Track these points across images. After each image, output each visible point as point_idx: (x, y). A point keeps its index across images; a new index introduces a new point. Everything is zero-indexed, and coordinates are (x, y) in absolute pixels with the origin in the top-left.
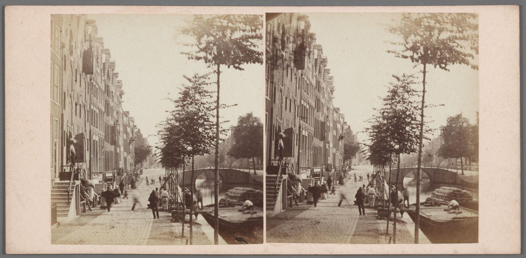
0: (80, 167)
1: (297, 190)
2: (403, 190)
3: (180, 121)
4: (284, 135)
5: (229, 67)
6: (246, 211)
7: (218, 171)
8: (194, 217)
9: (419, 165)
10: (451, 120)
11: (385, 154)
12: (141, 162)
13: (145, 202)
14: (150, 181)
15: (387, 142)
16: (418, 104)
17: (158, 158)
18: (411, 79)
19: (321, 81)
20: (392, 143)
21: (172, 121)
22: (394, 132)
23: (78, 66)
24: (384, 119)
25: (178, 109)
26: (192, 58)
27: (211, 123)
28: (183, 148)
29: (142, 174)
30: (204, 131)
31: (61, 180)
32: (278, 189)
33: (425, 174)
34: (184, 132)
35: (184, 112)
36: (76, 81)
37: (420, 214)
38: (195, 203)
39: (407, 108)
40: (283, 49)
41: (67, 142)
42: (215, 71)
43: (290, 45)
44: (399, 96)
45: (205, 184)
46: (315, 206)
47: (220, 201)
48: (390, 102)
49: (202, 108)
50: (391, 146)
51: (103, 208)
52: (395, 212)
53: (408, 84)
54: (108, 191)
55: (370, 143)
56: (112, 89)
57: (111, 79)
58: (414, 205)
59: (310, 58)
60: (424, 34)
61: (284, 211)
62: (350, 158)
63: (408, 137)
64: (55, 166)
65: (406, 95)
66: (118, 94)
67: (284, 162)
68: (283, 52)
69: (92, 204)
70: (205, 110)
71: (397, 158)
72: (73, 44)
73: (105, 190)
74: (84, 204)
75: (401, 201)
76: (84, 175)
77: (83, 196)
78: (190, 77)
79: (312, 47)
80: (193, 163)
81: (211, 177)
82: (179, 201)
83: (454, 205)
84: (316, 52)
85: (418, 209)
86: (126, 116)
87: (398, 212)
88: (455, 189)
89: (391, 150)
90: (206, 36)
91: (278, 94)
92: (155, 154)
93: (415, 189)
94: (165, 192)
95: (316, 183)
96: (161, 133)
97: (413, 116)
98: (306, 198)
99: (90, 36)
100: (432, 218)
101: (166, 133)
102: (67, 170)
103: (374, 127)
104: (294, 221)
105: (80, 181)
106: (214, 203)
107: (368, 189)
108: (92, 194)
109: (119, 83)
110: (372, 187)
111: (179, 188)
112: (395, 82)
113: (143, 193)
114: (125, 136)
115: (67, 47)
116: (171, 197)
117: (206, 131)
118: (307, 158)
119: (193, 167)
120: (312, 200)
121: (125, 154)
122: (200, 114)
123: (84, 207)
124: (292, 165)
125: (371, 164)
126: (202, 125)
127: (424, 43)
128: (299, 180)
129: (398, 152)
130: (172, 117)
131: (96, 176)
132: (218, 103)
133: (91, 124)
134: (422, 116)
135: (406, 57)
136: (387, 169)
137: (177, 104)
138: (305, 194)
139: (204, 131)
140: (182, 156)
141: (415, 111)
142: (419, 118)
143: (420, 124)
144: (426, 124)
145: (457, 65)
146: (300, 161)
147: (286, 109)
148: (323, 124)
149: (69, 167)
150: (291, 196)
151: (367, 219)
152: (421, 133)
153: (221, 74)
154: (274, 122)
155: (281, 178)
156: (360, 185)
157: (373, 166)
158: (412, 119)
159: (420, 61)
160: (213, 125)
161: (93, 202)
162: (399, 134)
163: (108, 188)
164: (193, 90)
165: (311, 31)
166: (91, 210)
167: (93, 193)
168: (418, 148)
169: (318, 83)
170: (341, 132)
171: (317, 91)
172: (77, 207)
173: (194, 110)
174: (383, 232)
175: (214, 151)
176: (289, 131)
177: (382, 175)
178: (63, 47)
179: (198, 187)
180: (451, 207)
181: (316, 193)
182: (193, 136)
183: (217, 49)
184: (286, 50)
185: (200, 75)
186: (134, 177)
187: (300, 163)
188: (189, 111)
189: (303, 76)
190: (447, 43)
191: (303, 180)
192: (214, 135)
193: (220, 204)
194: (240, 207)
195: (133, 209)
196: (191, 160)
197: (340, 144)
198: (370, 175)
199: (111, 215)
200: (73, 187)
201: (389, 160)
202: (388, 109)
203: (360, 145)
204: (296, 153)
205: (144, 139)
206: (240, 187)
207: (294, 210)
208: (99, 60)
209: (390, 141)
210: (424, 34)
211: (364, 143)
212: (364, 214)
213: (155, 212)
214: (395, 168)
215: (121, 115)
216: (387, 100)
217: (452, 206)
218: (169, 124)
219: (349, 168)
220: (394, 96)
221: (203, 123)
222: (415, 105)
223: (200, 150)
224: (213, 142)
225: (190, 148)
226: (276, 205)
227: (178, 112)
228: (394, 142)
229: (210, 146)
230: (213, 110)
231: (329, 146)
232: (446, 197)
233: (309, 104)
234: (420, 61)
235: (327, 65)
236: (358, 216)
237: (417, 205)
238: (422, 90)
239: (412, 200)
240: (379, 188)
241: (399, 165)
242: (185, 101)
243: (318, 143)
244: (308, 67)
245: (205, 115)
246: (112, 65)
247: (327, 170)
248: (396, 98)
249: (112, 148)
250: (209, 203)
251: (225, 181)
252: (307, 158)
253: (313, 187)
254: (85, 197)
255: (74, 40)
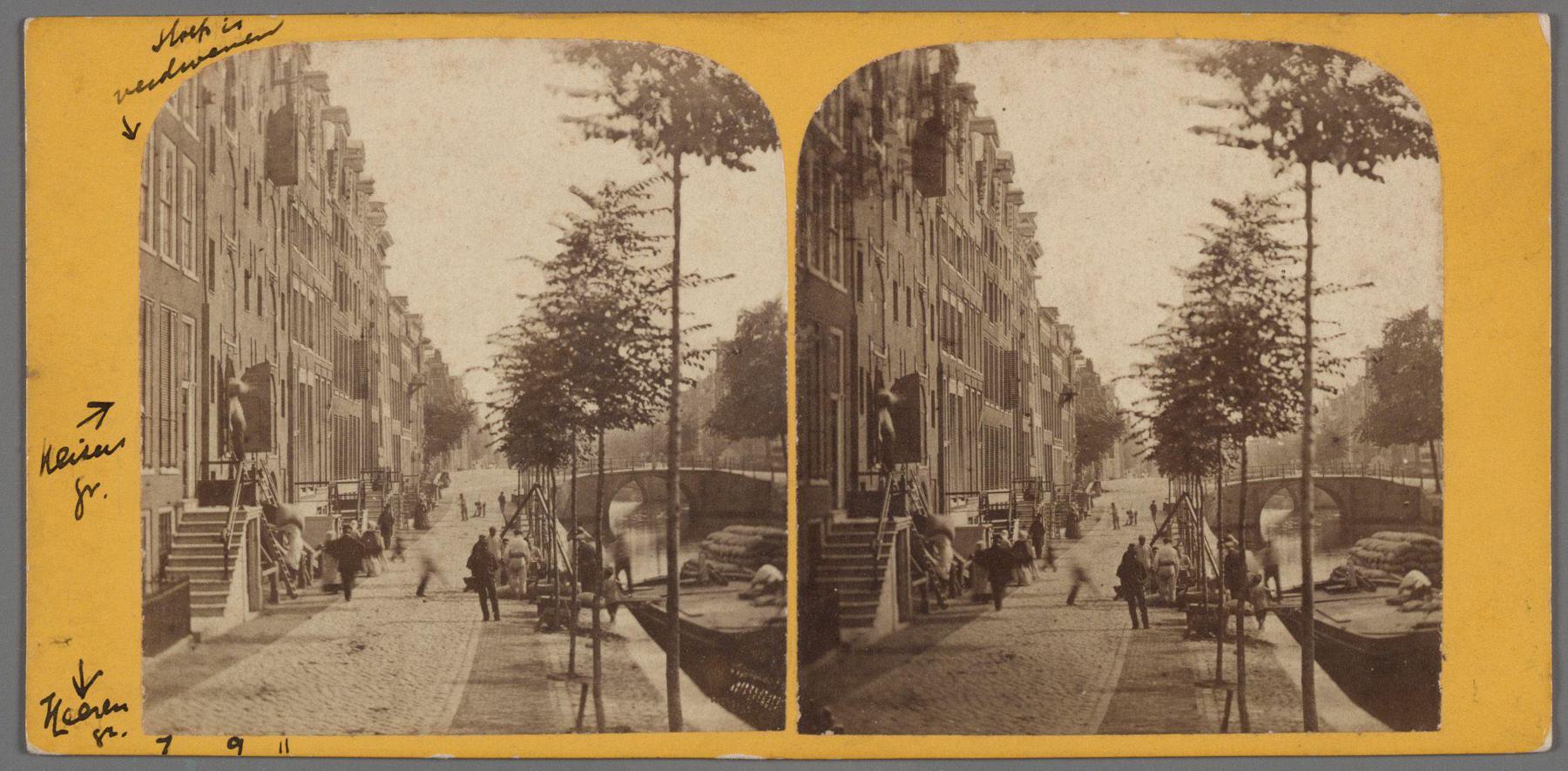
0: (259, 467)
1: (941, 562)
2: (1260, 545)
3: (561, 327)
4: (893, 398)
5: (708, 162)
6: (763, 599)
7: (678, 478)
8: (604, 615)
9: (1305, 469)
10: (1394, 331)
11: (1200, 440)
12: (445, 449)
13: (457, 571)
14: (471, 508)
15: (1204, 403)
16: (1295, 285)
17: (496, 438)
18: (1271, 210)
19: (999, 226)
20: (1220, 406)
21: (538, 325)
22: (1227, 365)
23: (252, 159)
24: (1193, 334)
25: (554, 288)
26: (597, 135)
27: (655, 332)
28: (572, 407)
29: (446, 486)
30: (635, 356)
31: (201, 505)
32: (885, 561)
33: (1326, 497)
34: (575, 360)
35: (572, 299)
36: (246, 204)
37: (1316, 616)
38: (609, 573)
39: (1261, 300)
40: (878, 136)
41: (222, 389)
42: (666, 174)
43: (900, 124)
44: (1236, 265)
45: (639, 517)
46: (998, 607)
47: (685, 568)
48: (1208, 282)
49: (626, 286)
50: (1219, 415)
51: (330, 589)
52: (1241, 614)
53: (1260, 224)
54: (344, 538)
55: (1151, 408)
56: (356, 228)
57: (352, 200)
58: (1295, 590)
59: (960, 161)
60: (1304, 73)
61: (904, 625)
62: (1097, 459)
63: (1269, 387)
64: (185, 462)
65: (1257, 261)
66: (373, 243)
67: (897, 479)
68: (878, 146)
69: (299, 576)
70: (636, 291)
71: (1239, 452)
72: (237, 93)
73: (335, 534)
74: (272, 576)
75: (1256, 580)
76: (271, 491)
77: (270, 555)
78: (592, 193)
79: (967, 125)
80: (601, 453)
81: (656, 497)
82: (561, 567)
83: (1418, 585)
84: (978, 140)
85: (1307, 602)
86: (399, 311)
87: (1248, 614)
88: (1419, 536)
89: (1222, 429)
90: (637, 68)
91: (869, 271)
92: (488, 426)
93: (1297, 543)
94: (518, 542)
95: (997, 538)
96: (506, 362)
97: (1281, 322)
98: (969, 584)
99: (288, 67)
100: (1351, 629)
101: (519, 362)
102: (222, 474)
103: (1164, 361)
104: (937, 656)
105: (260, 507)
106: (664, 573)
107: (1155, 549)
108: (297, 548)
109: (375, 210)
110: (1166, 542)
111: (560, 528)
112: (1221, 221)
113: (449, 544)
114: (395, 370)
115: (219, 100)
116: (536, 554)
117: (640, 356)
118: (967, 463)
119: (601, 463)
120: (988, 589)
121: (397, 424)
122: (622, 305)
123: (274, 587)
124: (923, 485)
125: (1162, 472)
126: (630, 336)
127: (1304, 98)
128: (945, 532)
129: (1240, 432)
130: (536, 314)
131: (310, 492)
132: (676, 272)
133: (293, 333)
134: (1308, 320)
135: (1250, 145)
136: (1210, 486)
137: (552, 273)
138: (966, 573)
139: (635, 356)
140: (569, 432)
141: (1286, 308)
142: (1298, 327)
143: (1301, 346)
144: (1322, 345)
145: (1405, 163)
146: (946, 476)
147: (896, 318)
148: (1011, 357)
149: (226, 467)
150: (924, 580)
151: (1155, 639)
152: (1307, 374)
153: (684, 183)
154: (862, 360)
155: (891, 525)
156: (1129, 537)
157: (1165, 479)
158: (1279, 333)
159: (1293, 155)
160: (663, 338)
161: (300, 572)
162: (1242, 378)
163: (346, 528)
164: (600, 231)
165: (961, 77)
166: (294, 597)
167: (299, 542)
168: (1299, 419)
169: (990, 236)
170: (1065, 379)
171: (987, 259)
172: (251, 588)
173: (604, 291)
174: (1205, 677)
175: (665, 416)
176: (908, 385)
177: (1195, 503)
178: (206, 99)
179: (617, 525)
180: (1407, 592)
181: (999, 568)
182: (601, 369)
183: (672, 107)
184: (887, 138)
185: (622, 184)
186: (423, 496)
187: (946, 481)
188: (588, 294)
189: (944, 216)
190: (1372, 95)
191: (957, 529)
192: (666, 368)
193: (683, 576)
194: (745, 587)
195: (420, 592)
196: (596, 443)
197: (1065, 415)
198: (1160, 507)
199: (355, 609)
200: (238, 527)
201: (1215, 458)
202: (1203, 304)
203: (1125, 416)
204: (933, 451)
205: (452, 381)
206: (745, 524)
207: (931, 621)
208: (316, 141)
209: (1216, 401)
210: (1304, 73)
211: (1138, 408)
212: (1146, 626)
213: (489, 602)
214: (1233, 481)
215: (382, 309)
216: (1200, 276)
217: (1411, 587)
218: (528, 334)
219: (1094, 488)
220: (1220, 263)
221: (631, 332)
222: (1282, 288)
223: (624, 414)
224: (661, 390)
225: (591, 408)
226: (880, 610)
227: (554, 298)
228: (1228, 403)
229: (652, 401)
230: (661, 291)
231: (1031, 425)
232: (1391, 563)
233: (963, 299)
234: (1293, 155)
235: (1014, 178)
236: (1128, 633)
237: (1305, 589)
238: (1304, 241)
239: (1291, 577)
240: (1188, 544)
241: (1244, 471)
242: (576, 265)
243: (996, 415)
244: (957, 187)
245: (638, 307)
246: (355, 157)
247: (1030, 497)
248: (1228, 268)
249: (355, 408)
250: (653, 575)
251: (700, 505)
252: (967, 463)
253: (988, 550)
254: (276, 557)
255: (240, 81)
